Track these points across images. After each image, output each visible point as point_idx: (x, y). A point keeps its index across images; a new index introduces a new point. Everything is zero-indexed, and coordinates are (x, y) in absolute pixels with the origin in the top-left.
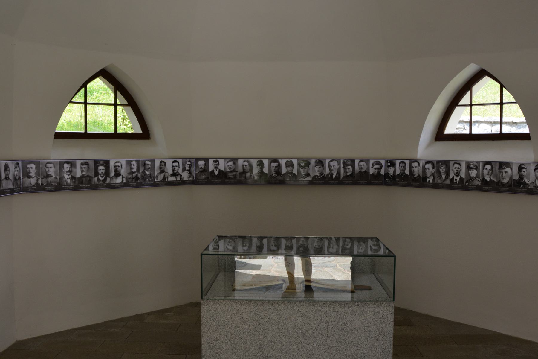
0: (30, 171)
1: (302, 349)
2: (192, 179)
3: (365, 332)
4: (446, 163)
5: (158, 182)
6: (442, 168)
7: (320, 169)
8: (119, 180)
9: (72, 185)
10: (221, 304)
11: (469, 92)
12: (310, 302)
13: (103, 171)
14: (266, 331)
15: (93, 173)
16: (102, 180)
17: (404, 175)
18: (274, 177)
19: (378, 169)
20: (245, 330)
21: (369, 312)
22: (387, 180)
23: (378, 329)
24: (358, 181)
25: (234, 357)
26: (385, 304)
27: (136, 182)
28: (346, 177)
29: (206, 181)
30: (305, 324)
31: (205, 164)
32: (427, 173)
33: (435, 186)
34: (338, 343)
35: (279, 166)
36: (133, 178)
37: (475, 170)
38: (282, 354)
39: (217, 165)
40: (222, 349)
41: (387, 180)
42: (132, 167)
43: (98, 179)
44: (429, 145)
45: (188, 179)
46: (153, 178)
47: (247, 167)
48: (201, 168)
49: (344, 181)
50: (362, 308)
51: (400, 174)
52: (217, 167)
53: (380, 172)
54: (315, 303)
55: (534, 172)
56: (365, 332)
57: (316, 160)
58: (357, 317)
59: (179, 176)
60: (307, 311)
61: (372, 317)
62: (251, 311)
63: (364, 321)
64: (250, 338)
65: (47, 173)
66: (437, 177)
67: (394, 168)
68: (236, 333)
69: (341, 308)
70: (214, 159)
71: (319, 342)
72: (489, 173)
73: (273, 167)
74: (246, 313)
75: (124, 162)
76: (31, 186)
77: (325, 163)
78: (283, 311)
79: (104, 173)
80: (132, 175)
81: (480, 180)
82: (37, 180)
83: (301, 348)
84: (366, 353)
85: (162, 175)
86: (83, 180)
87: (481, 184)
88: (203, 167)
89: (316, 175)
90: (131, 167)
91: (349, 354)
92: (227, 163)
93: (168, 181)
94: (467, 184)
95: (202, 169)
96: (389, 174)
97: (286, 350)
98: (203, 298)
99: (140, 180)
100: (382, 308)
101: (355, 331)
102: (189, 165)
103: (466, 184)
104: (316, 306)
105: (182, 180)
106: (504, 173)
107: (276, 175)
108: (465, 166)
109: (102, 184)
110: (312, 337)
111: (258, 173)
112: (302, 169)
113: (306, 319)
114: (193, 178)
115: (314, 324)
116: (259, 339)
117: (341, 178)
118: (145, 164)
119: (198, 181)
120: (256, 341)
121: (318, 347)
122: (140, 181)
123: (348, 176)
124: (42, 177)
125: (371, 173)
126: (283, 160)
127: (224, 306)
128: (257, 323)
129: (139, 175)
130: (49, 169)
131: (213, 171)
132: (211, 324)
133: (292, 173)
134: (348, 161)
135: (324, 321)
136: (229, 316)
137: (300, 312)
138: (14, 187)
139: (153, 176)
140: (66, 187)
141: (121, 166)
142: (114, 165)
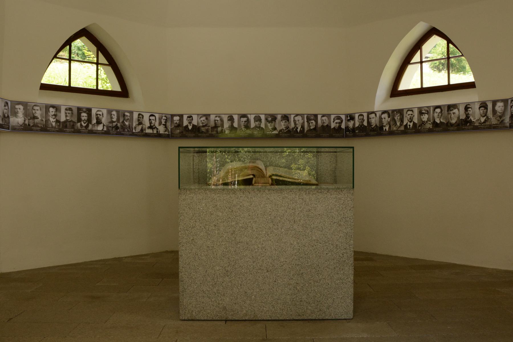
0: (18, 111)
1: (271, 235)
2: (168, 133)
3: (328, 218)
4: (400, 112)
5: (137, 132)
6: (397, 116)
7: (286, 123)
8: (100, 128)
9: (57, 128)
10: (197, 193)
11: (419, 51)
12: (278, 190)
13: (86, 118)
14: (238, 218)
15: (76, 119)
16: (84, 126)
17: (363, 126)
18: (243, 131)
19: (339, 123)
20: (218, 217)
21: (332, 198)
22: (347, 134)
23: (340, 214)
24: (321, 135)
25: (209, 243)
26: (345, 191)
27: (116, 131)
28: (310, 130)
29: (181, 135)
30: (273, 210)
31: (180, 119)
32: (383, 122)
33: (391, 133)
34: (304, 228)
35: (248, 121)
36: (114, 127)
37: (426, 115)
38: (252, 239)
39: (191, 120)
40: (197, 236)
41: (348, 133)
42: (112, 117)
43: (81, 125)
44: (385, 100)
45: (163, 133)
46: (131, 129)
47: (219, 122)
48: (176, 123)
49: (308, 135)
50: (324, 195)
51: (359, 126)
52: (191, 122)
53: (341, 125)
54: (282, 191)
55: (479, 110)
56: (328, 218)
57: (281, 115)
58: (320, 203)
59: (156, 129)
60: (275, 198)
61: (334, 203)
62: (224, 199)
63: (327, 207)
64: (224, 225)
65: (33, 114)
66: (393, 125)
67: (353, 121)
68: (210, 220)
69: (306, 195)
70: (188, 115)
71: (287, 227)
72: (439, 116)
73: (243, 121)
74: (220, 201)
75: (105, 112)
76: (19, 125)
77: (291, 118)
78: (254, 198)
79: (86, 119)
80: (113, 124)
81: (431, 123)
82: (25, 121)
83: (270, 233)
84: (330, 237)
85: (140, 127)
86: (67, 125)
87: (432, 126)
88: (178, 122)
89: (282, 129)
90: (111, 116)
91: (314, 238)
92: (200, 119)
93: (145, 133)
94: (419, 128)
95: (177, 124)
96: (349, 128)
97: (257, 235)
98: (181, 188)
99: (120, 129)
100: (343, 195)
101: (319, 216)
102: (165, 120)
103: (418, 128)
104: (283, 193)
105: (158, 133)
106: (452, 114)
107: (246, 129)
108: (418, 112)
109: (85, 130)
110: (280, 223)
111: (229, 127)
112: (269, 123)
113: (274, 205)
114: (169, 132)
115: (282, 210)
116: (231, 225)
117: (305, 131)
118: (124, 115)
119: (173, 135)
120: (229, 227)
121: (286, 232)
122: (119, 130)
123: (312, 129)
124: (29, 118)
125: (332, 127)
126: (251, 115)
127: (199, 195)
128: (230, 210)
129: (119, 125)
130: (36, 111)
131: (187, 126)
132: (187, 212)
133: (260, 127)
134: (312, 116)
135: (291, 208)
136: (204, 204)
137: (269, 199)
138: (3, 124)
139: (132, 127)
140: (51, 129)
141: (103, 114)
142: (96, 114)
